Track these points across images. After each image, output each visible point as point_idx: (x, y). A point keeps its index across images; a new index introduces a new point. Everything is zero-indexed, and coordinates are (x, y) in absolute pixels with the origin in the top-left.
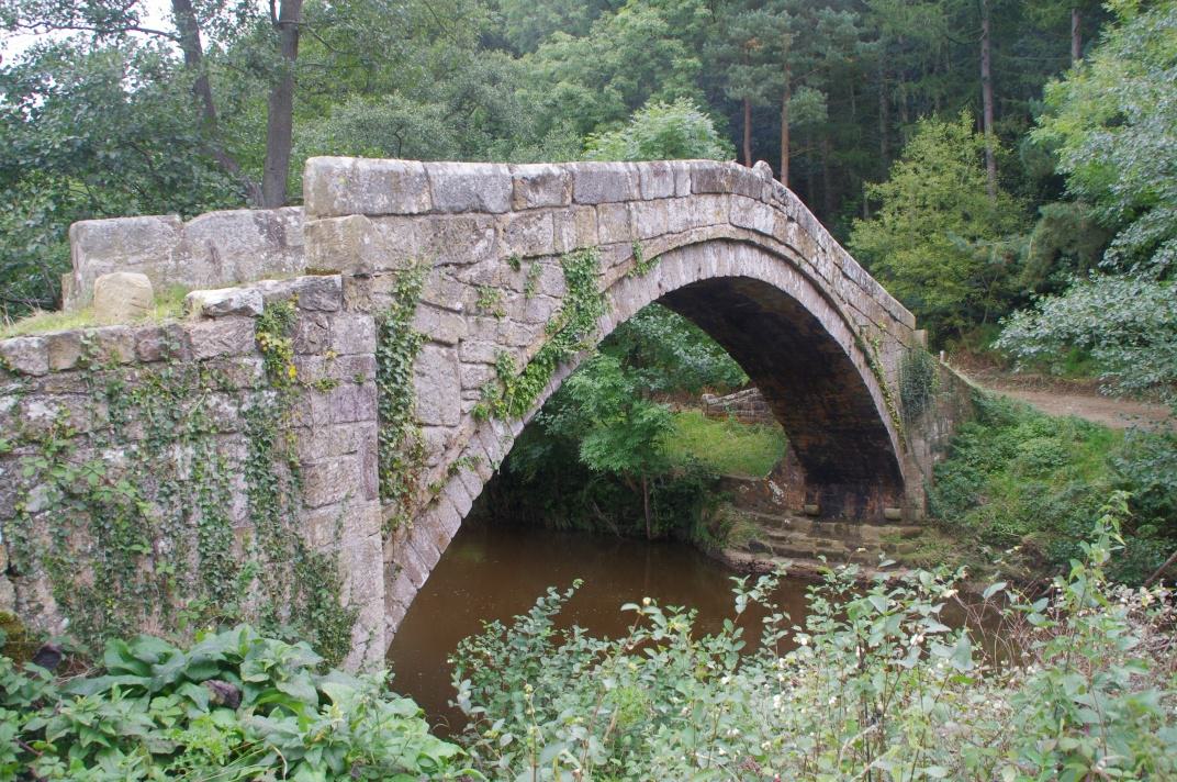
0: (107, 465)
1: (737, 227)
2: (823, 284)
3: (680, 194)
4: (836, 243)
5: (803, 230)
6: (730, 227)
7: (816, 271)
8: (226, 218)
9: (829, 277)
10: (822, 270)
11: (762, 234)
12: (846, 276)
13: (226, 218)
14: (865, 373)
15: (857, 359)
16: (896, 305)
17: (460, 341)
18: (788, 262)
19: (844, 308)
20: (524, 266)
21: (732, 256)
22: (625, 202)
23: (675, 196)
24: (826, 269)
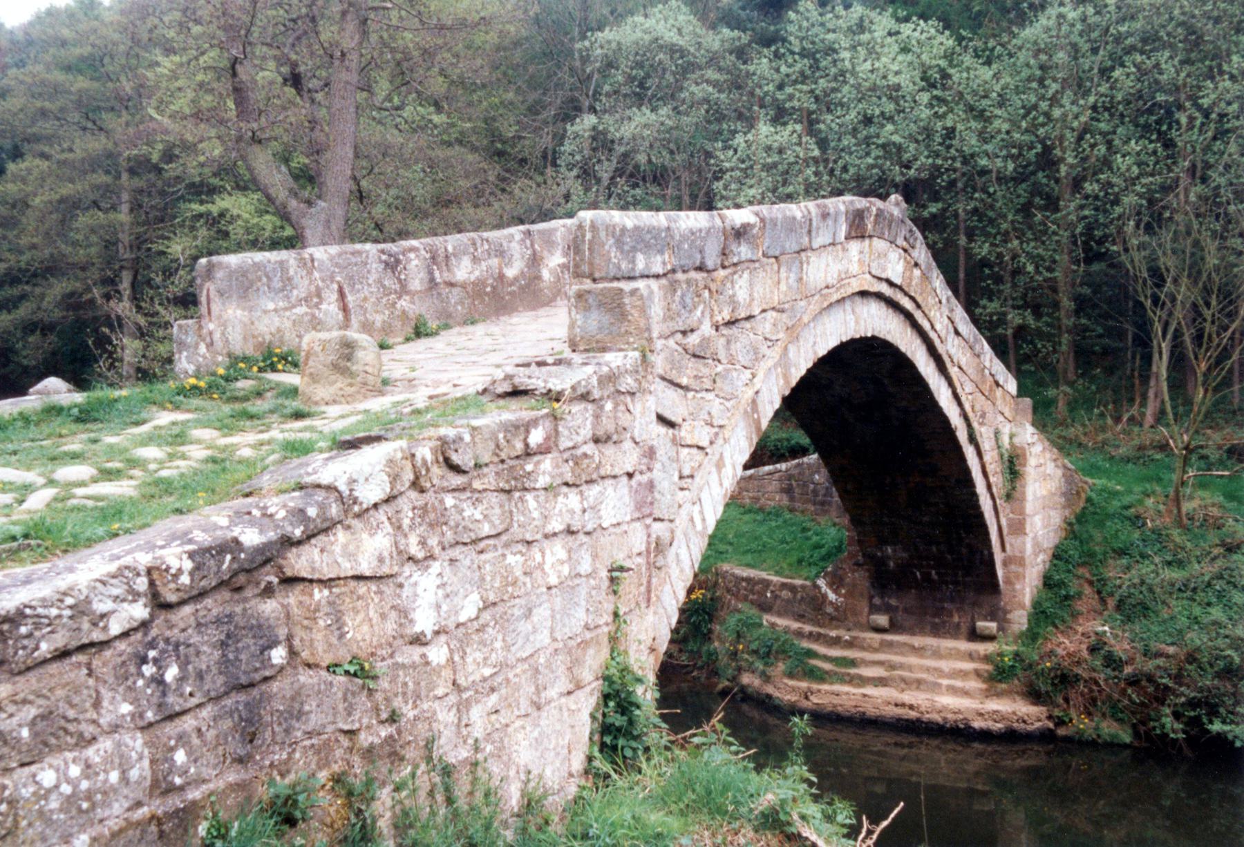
0: (181, 679)
1: (874, 276)
2: (937, 342)
3: (837, 241)
4: (950, 293)
5: (925, 277)
6: (868, 276)
7: (933, 327)
8: (353, 254)
9: (943, 335)
10: (938, 327)
11: (891, 284)
12: (957, 333)
13: (353, 254)
14: (969, 452)
15: (962, 436)
16: (644, 240)
17: (478, 466)
18: (908, 316)
19: (953, 371)
20: (725, 331)
21: (865, 310)
22: (798, 252)
23: (833, 244)
24: (941, 324)
